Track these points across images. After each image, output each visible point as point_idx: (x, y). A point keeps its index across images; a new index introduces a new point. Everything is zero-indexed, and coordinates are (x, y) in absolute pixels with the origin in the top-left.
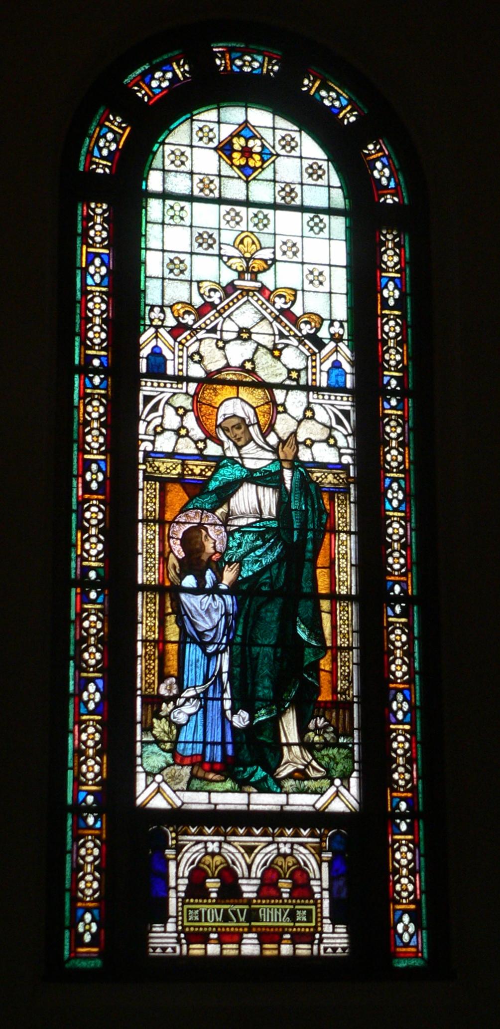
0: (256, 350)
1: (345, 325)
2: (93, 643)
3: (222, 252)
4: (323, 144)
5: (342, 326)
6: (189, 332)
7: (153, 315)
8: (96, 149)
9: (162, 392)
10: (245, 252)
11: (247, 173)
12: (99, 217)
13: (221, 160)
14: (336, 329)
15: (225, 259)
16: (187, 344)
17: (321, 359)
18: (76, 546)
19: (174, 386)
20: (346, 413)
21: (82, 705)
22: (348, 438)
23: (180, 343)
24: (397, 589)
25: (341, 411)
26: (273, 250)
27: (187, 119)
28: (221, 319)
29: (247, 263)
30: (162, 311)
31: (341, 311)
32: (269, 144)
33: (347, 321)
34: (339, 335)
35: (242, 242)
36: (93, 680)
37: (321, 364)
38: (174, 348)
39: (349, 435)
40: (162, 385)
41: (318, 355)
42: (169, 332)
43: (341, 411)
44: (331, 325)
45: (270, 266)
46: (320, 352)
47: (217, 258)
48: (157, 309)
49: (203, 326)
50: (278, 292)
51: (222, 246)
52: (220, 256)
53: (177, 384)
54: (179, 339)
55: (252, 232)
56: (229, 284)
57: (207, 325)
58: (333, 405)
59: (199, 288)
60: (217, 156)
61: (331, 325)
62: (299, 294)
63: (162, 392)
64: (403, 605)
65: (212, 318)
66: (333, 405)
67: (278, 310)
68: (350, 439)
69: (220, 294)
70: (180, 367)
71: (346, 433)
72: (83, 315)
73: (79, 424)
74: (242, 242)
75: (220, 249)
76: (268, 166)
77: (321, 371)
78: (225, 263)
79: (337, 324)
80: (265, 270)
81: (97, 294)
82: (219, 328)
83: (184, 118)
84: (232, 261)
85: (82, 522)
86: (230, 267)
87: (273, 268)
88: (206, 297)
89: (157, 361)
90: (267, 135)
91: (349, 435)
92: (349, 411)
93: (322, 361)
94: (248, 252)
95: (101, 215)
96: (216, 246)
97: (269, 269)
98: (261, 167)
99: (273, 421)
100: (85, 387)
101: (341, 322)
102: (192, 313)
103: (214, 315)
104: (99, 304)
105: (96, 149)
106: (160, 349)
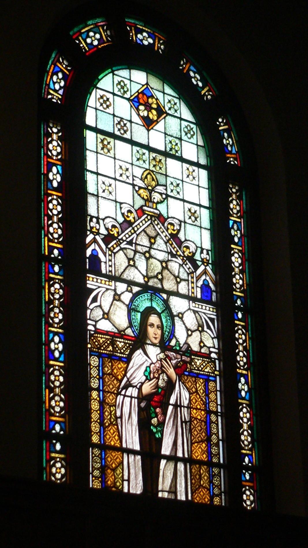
0: (145, 232)
1: (210, 252)
2: (56, 305)
3: (135, 183)
4: (193, 112)
5: (208, 254)
6: (115, 241)
7: (92, 224)
8: (51, 82)
9: (99, 287)
10: (149, 186)
11: (148, 123)
12: (56, 305)
13: (132, 108)
14: (204, 255)
15: (137, 188)
16: (115, 251)
17: (196, 277)
18: (45, 402)
19: (107, 283)
20: (212, 320)
21: (52, 445)
22: (214, 339)
23: (110, 249)
24: (247, 460)
25: (209, 318)
26: (165, 188)
27: (109, 73)
28: (135, 235)
29: (150, 193)
30: (98, 222)
31: (207, 244)
32: (141, 88)
33: (211, 251)
34: (207, 260)
35: (146, 177)
36: (56, 165)
37: (197, 281)
38: (106, 253)
39: (215, 338)
40: (99, 281)
41: (195, 273)
42: (102, 239)
43: (209, 318)
44: (202, 252)
45: (164, 199)
46: (195, 272)
47: (131, 187)
48: (94, 220)
49: (124, 238)
50: (170, 220)
51: (134, 178)
52: (134, 185)
53: (109, 281)
54: (109, 246)
55: (153, 171)
56: (139, 209)
57: (127, 238)
58: (204, 313)
59: (121, 208)
60: (130, 106)
61: (202, 252)
62: (183, 224)
63: (99, 287)
64: (244, 464)
65: (130, 234)
66: (204, 313)
67: (169, 234)
68: (216, 341)
69: (135, 214)
70: (110, 269)
71: (213, 336)
72: (46, 213)
73: (46, 302)
74: (146, 177)
75: (133, 180)
76: (135, 93)
77: (197, 287)
78: (137, 191)
79: (205, 251)
80: (161, 202)
81: (57, 414)
82: (134, 241)
83: (107, 72)
84: (141, 191)
85: (49, 383)
86: (139, 195)
87: (166, 201)
88: (125, 217)
89: (95, 259)
90: (160, 95)
91: (215, 338)
92: (214, 319)
93: (197, 278)
94: (150, 186)
95: (58, 299)
96: (131, 178)
97: (164, 201)
98: (157, 120)
99: (162, 298)
100: (49, 273)
101: (208, 251)
102: (117, 227)
103: (130, 231)
104: (56, 147)
105: (51, 82)
106: (97, 253)
